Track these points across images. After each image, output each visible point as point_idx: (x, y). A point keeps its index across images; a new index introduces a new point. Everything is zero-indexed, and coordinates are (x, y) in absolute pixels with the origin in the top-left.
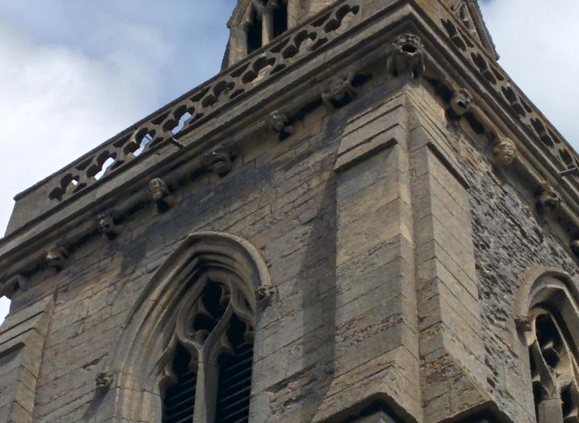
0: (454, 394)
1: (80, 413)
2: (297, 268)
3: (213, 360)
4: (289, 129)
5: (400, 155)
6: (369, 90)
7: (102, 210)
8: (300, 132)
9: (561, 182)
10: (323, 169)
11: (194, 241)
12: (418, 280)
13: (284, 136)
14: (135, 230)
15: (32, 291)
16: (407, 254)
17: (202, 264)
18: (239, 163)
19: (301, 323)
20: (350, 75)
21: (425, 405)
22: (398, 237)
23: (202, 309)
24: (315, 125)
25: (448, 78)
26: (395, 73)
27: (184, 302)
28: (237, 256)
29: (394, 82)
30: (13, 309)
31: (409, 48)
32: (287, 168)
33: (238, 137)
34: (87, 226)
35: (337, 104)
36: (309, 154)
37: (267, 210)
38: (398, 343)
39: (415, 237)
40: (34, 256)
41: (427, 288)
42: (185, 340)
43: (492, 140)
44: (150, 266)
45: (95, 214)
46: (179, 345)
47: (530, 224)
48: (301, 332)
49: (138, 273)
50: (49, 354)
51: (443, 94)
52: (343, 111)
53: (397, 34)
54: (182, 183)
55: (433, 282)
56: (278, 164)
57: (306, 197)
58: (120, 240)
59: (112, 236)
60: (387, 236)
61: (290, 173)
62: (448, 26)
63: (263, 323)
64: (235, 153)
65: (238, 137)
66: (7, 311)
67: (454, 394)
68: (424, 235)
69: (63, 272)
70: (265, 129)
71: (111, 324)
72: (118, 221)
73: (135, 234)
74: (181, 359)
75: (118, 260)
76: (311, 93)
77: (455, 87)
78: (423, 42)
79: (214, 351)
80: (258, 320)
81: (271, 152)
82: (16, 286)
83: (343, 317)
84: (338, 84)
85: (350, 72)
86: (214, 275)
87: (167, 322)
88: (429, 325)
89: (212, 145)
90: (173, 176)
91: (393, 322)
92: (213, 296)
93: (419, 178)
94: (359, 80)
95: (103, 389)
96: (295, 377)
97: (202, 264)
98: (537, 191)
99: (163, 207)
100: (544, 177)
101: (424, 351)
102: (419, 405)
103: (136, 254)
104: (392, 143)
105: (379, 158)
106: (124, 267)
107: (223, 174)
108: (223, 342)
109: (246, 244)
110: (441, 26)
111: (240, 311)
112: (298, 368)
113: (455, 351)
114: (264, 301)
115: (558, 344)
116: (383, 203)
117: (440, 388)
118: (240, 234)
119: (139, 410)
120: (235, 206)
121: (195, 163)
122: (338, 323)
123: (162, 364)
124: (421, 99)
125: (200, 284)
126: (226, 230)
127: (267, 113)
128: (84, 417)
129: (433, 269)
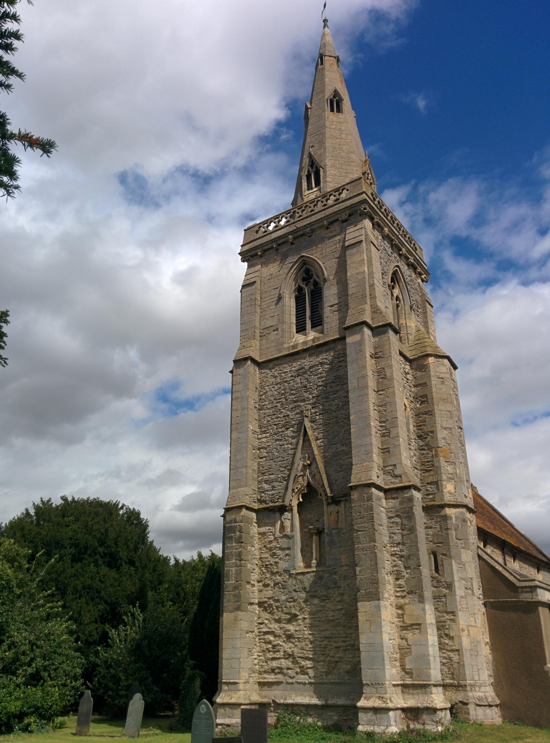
0: (380, 317)
1: (274, 303)
2: (334, 272)
3: (309, 292)
4: (329, 226)
5: (364, 244)
6: (352, 219)
7: (274, 242)
8: (332, 229)
9: (398, 237)
10: (340, 242)
11: (302, 256)
12: (369, 283)
13: (327, 228)
14: (284, 249)
15: (254, 262)
16: (367, 276)
17: (304, 263)
18: (314, 234)
19: (336, 289)
20: (348, 214)
21: (372, 319)
22: (364, 271)
23: (305, 275)
24: (336, 227)
25: (373, 215)
26: (360, 215)
27: (300, 273)
28: (316, 263)
29: (360, 218)
30: (249, 267)
31: (365, 209)
32: (329, 239)
33: (314, 227)
34: (270, 246)
35: (343, 222)
36: (336, 236)
37: (324, 251)
38: (366, 303)
39: (368, 270)
40: (254, 252)
41: (372, 286)
42: (301, 285)
43: (383, 229)
44: (290, 262)
45: (272, 243)
46: (299, 285)
47: (390, 250)
48: (336, 292)
49: (286, 263)
50: (262, 284)
51: (372, 219)
52: (345, 224)
53: (362, 204)
54: (297, 237)
55: (373, 284)
56: (326, 237)
57: (335, 250)
58: (279, 251)
59: (277, 250)
60: (361, 270)
61: (330, 241)
62: (372, 194)
63: (325, 286)
64: (313, 231)
65: (314, 227)
66: (246, 267)
67: (380, 317)
68: (370, 270)
69: (263, 258)
70: (322, 225)
71: (280, 277)
72: (279, 245)
73: (284, 250)
74: (299, 290)
75: (279, 258)
76: (336, 217)
77: (375, 217)
78: (369, 207)
79: (310, 289)
80: (324, 285)
81: (323, 233)
82: (249, 260)
83: (350, 292)
84: (344, 216)
85: (348, 213)
86: (308, 267)
87: (296, 280)
88: (373, 297)
89: (307, 227)
90: (295, 235)
91: (364, 296)
92: (307, 271)
93: (369, 252)
94: (350, 215)
95: (280, 298)
96: (336, 304)
97: (304, 263)
98: (392, 240)
99: (292, 244)
100: (394, 236)
101: (372, 304)
102: (371, 319)
103: (284, 258)
104: (362, 241)
105: (358, 244)
106: (282, 260)
107: (309, 237)
108: (312, 287)
109: (319, 261)
110: (370, 196)
111: (317, 279)
112: (337, 302)
113: (379, 304)
114: (325, 280)
115: (395, 283)
116: (359, 259)
117: (376, 315)
118: (316, 257)
119: (290, 303)
120: (314, 248)
121: (301, 232)
122: (349, 293)
123: (295, 291)
124: (367, 223)
125: (304, 268)
126: (312, 255)
127: (323, 221)
128: (213, 218)
129: (373, 281)
